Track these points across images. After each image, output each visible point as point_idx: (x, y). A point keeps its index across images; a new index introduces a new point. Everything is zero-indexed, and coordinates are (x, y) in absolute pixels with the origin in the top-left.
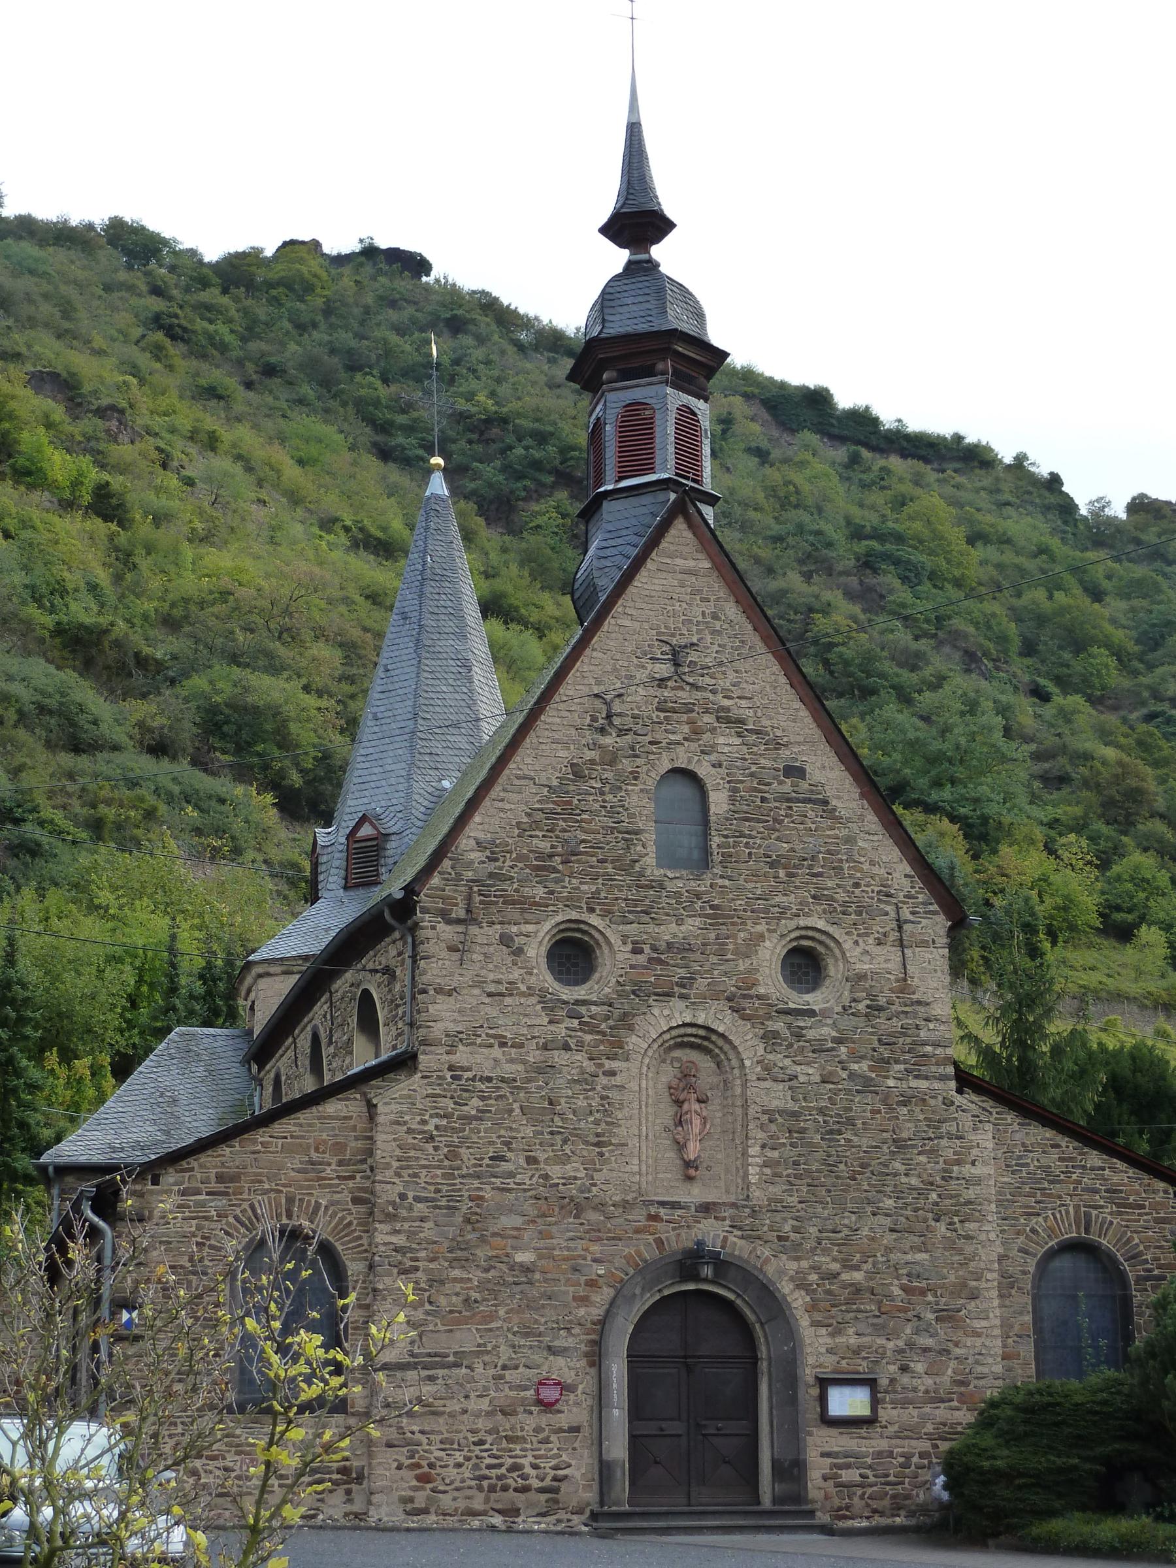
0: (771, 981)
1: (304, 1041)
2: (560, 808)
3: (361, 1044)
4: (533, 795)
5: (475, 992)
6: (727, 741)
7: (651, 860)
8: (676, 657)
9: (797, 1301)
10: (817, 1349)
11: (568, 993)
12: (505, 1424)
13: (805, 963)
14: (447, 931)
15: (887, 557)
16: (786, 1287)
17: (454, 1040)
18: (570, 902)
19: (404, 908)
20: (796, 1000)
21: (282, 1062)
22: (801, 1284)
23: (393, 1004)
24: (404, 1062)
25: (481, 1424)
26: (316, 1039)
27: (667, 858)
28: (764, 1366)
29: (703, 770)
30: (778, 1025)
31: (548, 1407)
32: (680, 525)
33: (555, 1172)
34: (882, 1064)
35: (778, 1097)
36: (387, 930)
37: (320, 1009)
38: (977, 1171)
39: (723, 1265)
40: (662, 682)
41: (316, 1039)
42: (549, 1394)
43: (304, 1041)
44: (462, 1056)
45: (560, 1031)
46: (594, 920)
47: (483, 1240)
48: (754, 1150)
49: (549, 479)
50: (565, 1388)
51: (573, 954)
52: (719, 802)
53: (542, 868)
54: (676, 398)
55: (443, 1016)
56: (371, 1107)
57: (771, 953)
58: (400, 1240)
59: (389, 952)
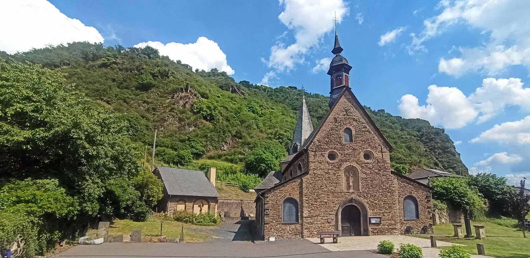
0: (362, 159)
1: (289, 171)
2: (328, 136)
3: (298, 171)
4: (325, 132)
5: (317, 162)
6: (355, 123)
7: (343, 141)
8: (346, 111)
9: (367, 206)
10: (370, 213)
11: (331, 162)
12: (323, 225)
13: (367, 156)
14: (313, 153)
15: (288, 131)
16: (365, 204)
17: (314, 169)
18: (331, 148)
19: (305, 152)
20: (366, 161)
21: (286, 174)
22: (368, 203)
23: (304, 165)
24: (307, 173)
25: (319, 225)
26: (291, 171)
27: (346, 141)
28: (362, 216)
29: (351, 128)
30: (364, 165)
31: (329, 223)
32: (347, 91)
33: (330, 188)
34: (379, 170)
35: (364, 176)
36: (303, 154)
37: (292, 167)
38: (395, 185)
39: (356, 201)
40: (345, 115)
41: (291, 171)
42: (329, 221)
43: (289, 171)
44: (315, 172)
45: (330, 167)
46: (335, 151)
47: (319, 198)
48: (360, 184)
49: (335, 96)
50: (332, 220)
51: (332, 156)
52: (354, 133)
53: (327, 143)
54: (344, 74)
55: (312, 166)
56: (302, 180)
57: (362, 154)
58: (307, 199)
59: (303, 157)
